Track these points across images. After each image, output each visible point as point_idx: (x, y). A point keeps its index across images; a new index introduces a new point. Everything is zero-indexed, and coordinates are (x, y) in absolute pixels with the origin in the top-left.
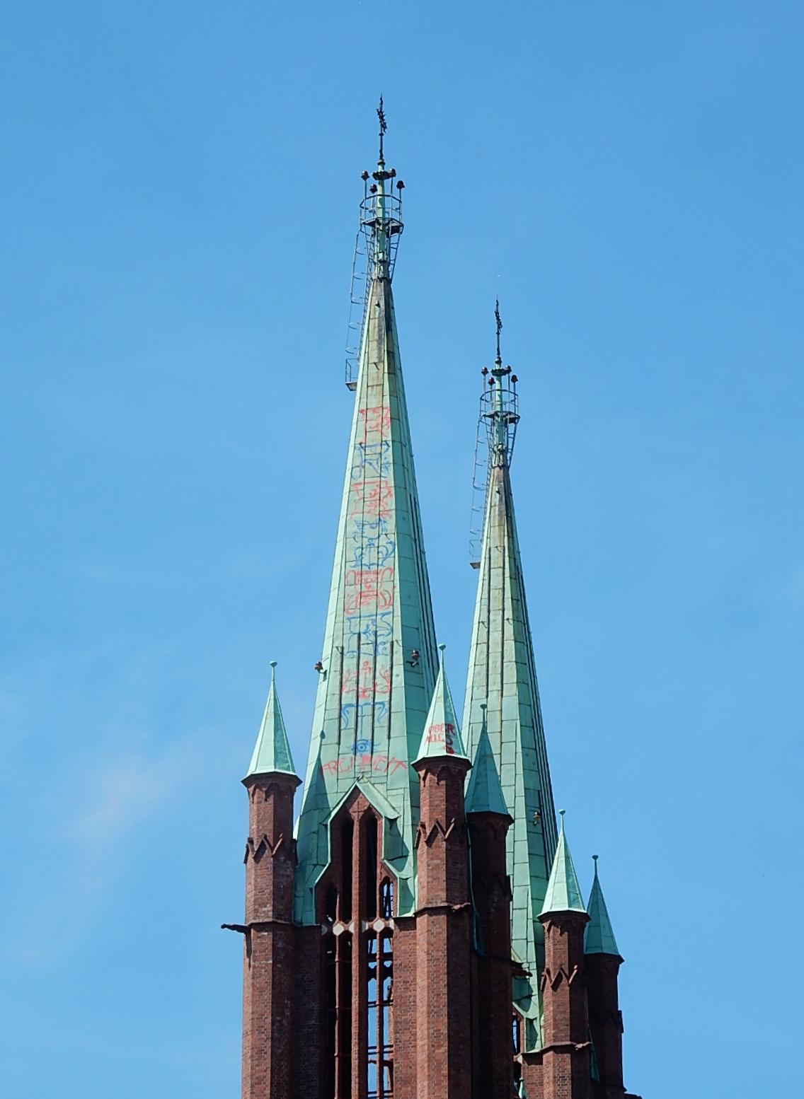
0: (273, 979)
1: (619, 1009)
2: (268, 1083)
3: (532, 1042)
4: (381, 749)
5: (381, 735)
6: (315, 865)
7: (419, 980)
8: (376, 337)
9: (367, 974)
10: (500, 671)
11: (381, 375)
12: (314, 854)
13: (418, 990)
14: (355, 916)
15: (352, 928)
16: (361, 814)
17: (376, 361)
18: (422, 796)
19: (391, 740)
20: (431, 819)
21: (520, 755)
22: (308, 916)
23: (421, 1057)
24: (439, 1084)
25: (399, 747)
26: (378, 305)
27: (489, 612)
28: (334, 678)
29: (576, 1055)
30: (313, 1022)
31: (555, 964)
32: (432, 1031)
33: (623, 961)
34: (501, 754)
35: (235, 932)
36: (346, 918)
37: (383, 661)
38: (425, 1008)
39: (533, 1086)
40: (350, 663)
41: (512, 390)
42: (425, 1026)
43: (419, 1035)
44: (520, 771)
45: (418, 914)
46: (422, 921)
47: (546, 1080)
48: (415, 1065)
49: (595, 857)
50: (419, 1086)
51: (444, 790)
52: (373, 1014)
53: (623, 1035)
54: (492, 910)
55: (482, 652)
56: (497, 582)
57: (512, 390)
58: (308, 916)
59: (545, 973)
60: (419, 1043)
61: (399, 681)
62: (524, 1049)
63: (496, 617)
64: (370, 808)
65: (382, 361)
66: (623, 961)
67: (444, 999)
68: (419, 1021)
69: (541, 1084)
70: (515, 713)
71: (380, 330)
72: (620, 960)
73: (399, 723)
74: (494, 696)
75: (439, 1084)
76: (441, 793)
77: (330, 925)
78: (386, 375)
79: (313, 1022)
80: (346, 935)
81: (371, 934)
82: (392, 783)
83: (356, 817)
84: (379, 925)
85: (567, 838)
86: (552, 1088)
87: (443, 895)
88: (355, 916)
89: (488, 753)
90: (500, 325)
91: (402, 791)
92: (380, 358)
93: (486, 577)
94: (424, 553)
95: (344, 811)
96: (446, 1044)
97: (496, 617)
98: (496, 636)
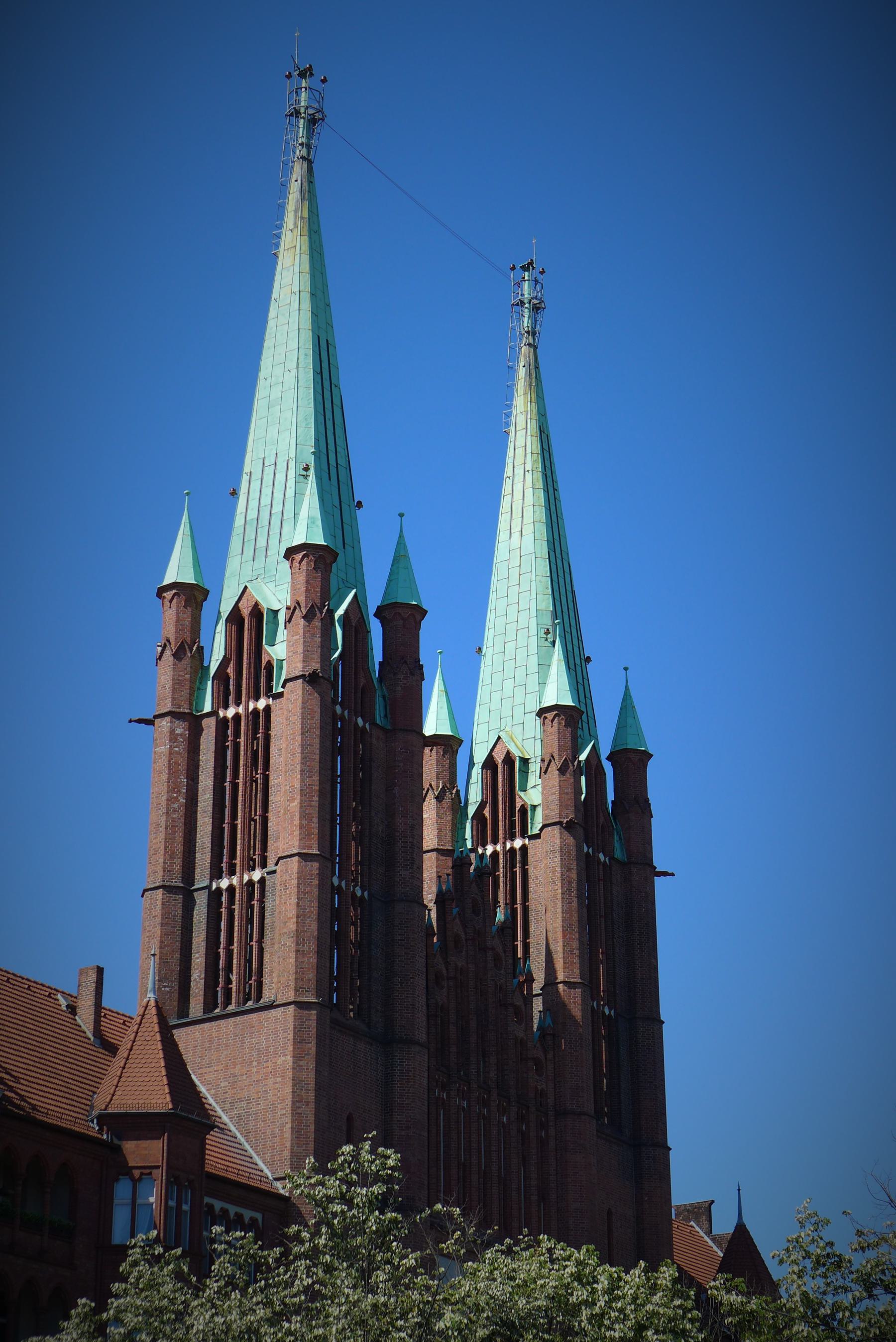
0: (170, 761)
17: (292, 227)
24: (309, 835)
37: (280, 477)
49: (626, 669)
54: (399, 688)
64: (257, 604)
65: (296, 226)
67: (298, 757)
72: (648, 756)
83: (246, 612)
95: (236, 610)
96: (299, 797)
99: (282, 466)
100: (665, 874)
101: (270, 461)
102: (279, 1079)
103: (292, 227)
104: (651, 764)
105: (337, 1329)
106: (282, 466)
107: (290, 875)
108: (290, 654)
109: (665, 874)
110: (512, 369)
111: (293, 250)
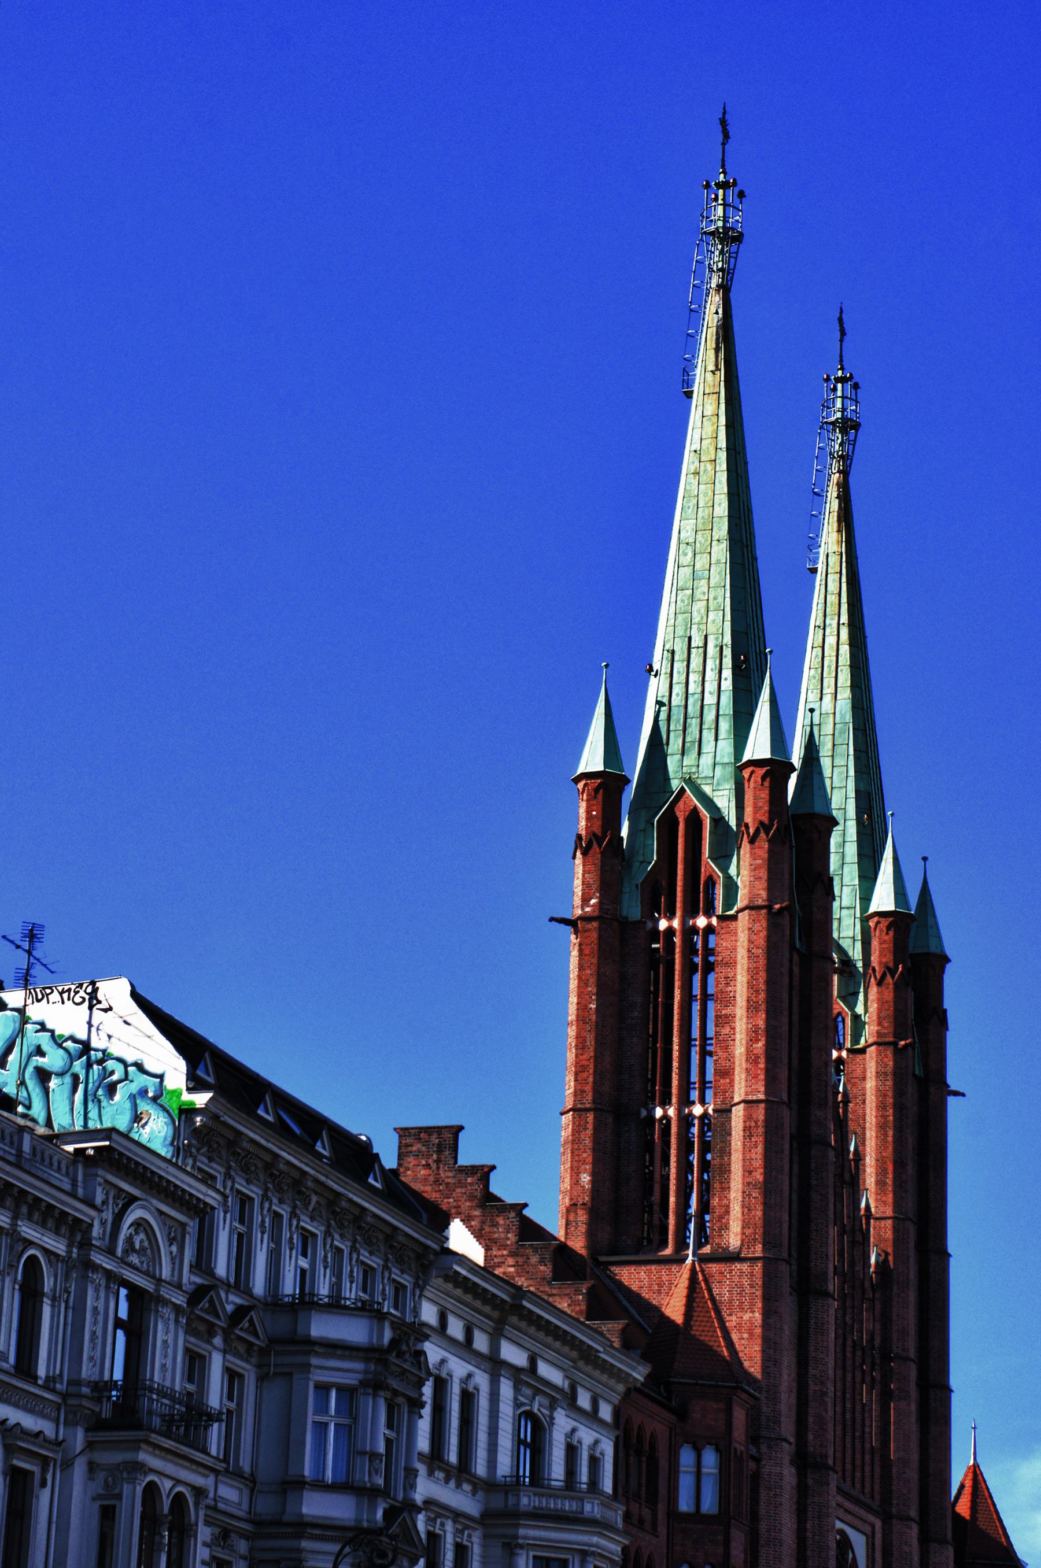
1: (375, 1151)
2: (591, 1071)
3: (856, 1039)
4: (708, 746)
5: (708, 736)
6: (642, 862)
7: (739, 977)
8: (714, 346)
9: (690, 969)
10: (834, 675)
11: (717, 383)
12: (641, 852)
13: (738, 985)
14: (678, 913)
15: (676, 924)
16: (687, 813)
18: (746, 797)
19: (719, 742)
20: (754, 819)
21: (851, 758)
22: (633, 910)
23: (739, 1050)
25: (726, 747)
26: (717, 313)
27: (825, 616)
28: (664, 679)
29: (898, 1052)
30: (636, 1014)
31: (880, 963)
32: (750, 1026)
33: (949, 961)
34: (833, 756)
35: (562, 925)
36: (671, 916)
38: (744, 1003)
39: (857, 1080)
40: (679, 666)
41: (854, 397)
42: (744, 1020)
43: (738, 1030)
44: (852, 772)
45: (738, 912)
46: (744, 918)
47: (869, 1074)
48: (733, 1057)
50: (737, 1078)
51: (767, 792)
52: (696, 1007)
53: (948, 1033)
55: (817, 656)
56: (833, 587)
57: (854, 397)
58: (633, 910)
59: (870, 971)
60: (738, 1036)
61: (727, 685)
62: (848, 1045)
63: (832, 622)
65: (718, 368)
66: (949, 961)
68: (738, 1017)
69: (864, 1079)
70: (849, 717)
71: (717, 339)
72: (948, 960)
73: (725, 725)
74: (828, 699)
75: (756, 1077)
76: (765, 795)
77: (657, 920)
78: (722, 384)
79: (636, 1014)
80: (670, 931)
81: (695, 930)
82: (718, 784)
84: (701, 922)
85: (735, 311)
86: (874, 1083)
87: (764, 894)
88: (678, 913)
89: (815, 756)
90: (843, 333)
91: (726, 792)
92: (717, 365)
93: (823, 582)
94: (756, 559)
97: (832, 622)
98: (831, 640)
99: (712, 651)
100: (956, 1094)
101: (698, 641)
102: (746, 1336)
103: (713, 368)
104: (949, 968)
105: (92, 1399)
106: (712, 651)
107: (756, 1122)
108: (752, 879)
109: (956, 1094)
110: (819, 496)
111: (716, 396)
